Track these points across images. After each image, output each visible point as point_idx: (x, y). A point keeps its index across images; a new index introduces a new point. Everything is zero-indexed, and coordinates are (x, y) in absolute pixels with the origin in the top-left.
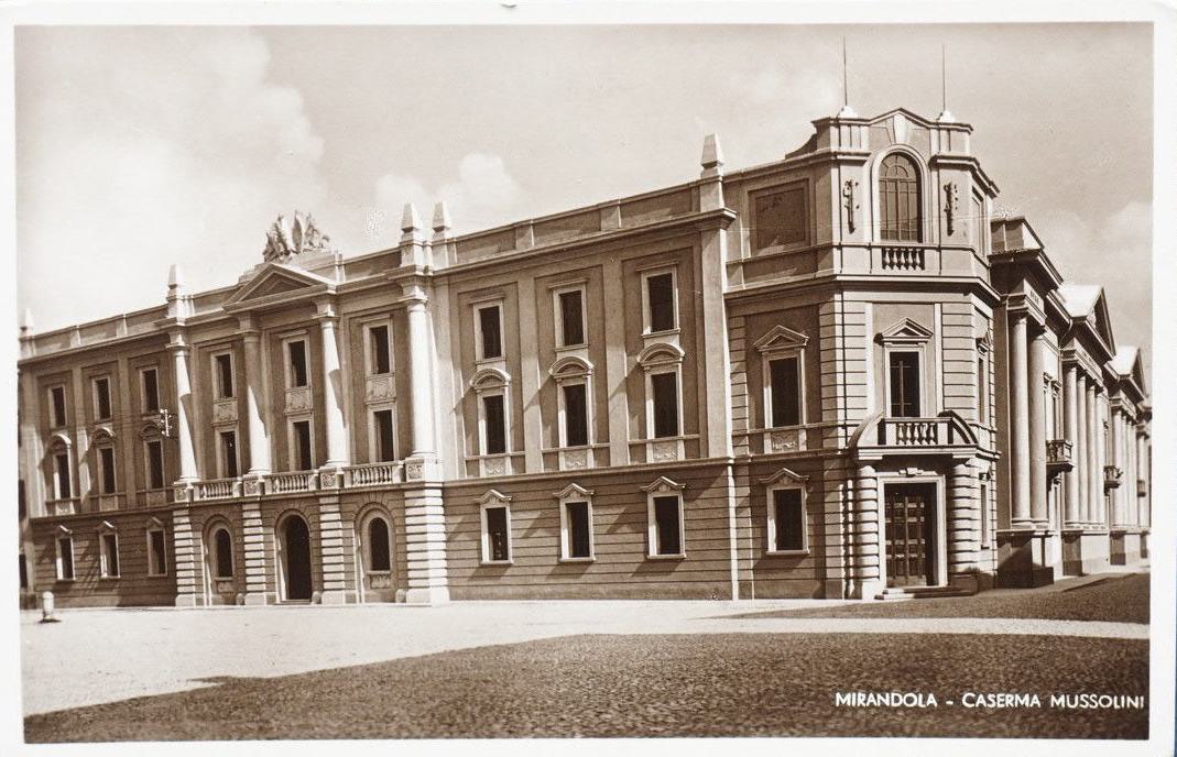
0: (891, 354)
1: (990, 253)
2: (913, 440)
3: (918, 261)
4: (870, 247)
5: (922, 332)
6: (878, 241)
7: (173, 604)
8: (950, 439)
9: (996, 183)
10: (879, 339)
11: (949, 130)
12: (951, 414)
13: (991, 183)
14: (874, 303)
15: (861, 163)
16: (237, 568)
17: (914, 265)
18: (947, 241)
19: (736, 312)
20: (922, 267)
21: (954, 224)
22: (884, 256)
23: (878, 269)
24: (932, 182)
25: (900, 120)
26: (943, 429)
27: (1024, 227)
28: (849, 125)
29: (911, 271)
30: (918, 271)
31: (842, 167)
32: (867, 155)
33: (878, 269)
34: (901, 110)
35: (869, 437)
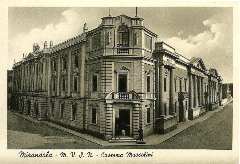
0: (119, 75)
1: (154, 50)
2: (122, 98)
3: (127, 52)
4: (113, 48)
5: (127, 70)
6: (116, 46)
7: (231, 86)
8: (133, 98)
9: (155, 33)
10: (115, 72)
11: (110, 19)
12: (133, 91)
13: (154, 34)
14: (114, 62)
15: (111, 28)
16: (60, 109)
17: (126, 53)
18: (135, 47)
19: (88, 63)
20: (128, 53)
21: (173, 48)
22: (118, 50)
23: (116, 54)
24: (131, 34)
25: (123, 18)
26: (131, 95)
27: (163, 44)
28: (112, 19)
29: (121, 54)
30: (127, 54)
31: (107, 49)
32: (114, 26)
33: (116, 54)
34: (124, 16)
35: (109, 97)
